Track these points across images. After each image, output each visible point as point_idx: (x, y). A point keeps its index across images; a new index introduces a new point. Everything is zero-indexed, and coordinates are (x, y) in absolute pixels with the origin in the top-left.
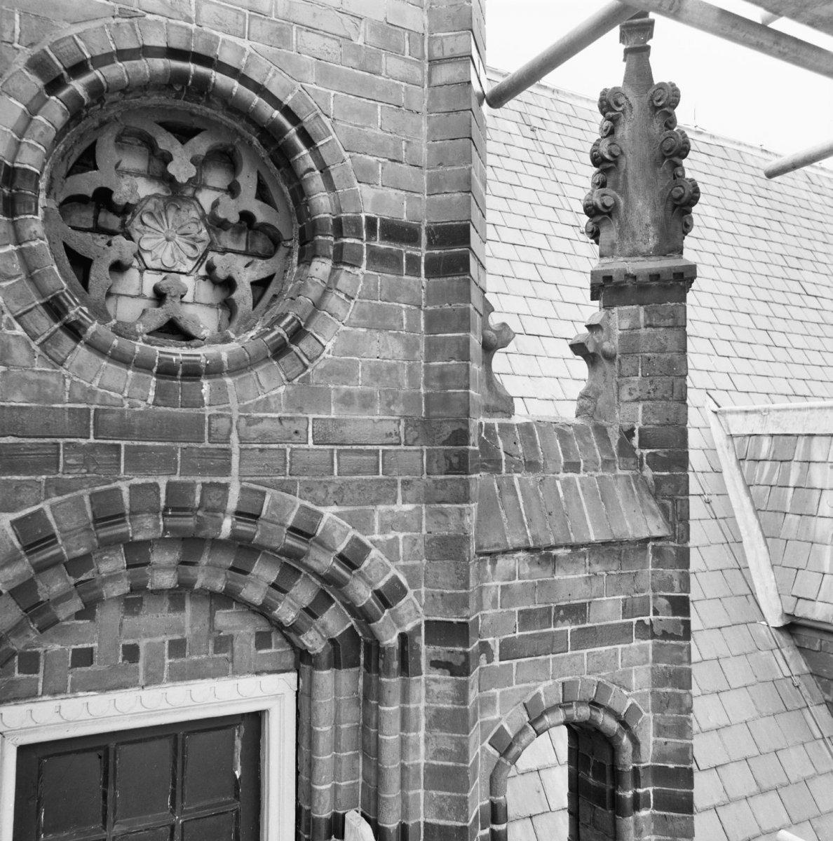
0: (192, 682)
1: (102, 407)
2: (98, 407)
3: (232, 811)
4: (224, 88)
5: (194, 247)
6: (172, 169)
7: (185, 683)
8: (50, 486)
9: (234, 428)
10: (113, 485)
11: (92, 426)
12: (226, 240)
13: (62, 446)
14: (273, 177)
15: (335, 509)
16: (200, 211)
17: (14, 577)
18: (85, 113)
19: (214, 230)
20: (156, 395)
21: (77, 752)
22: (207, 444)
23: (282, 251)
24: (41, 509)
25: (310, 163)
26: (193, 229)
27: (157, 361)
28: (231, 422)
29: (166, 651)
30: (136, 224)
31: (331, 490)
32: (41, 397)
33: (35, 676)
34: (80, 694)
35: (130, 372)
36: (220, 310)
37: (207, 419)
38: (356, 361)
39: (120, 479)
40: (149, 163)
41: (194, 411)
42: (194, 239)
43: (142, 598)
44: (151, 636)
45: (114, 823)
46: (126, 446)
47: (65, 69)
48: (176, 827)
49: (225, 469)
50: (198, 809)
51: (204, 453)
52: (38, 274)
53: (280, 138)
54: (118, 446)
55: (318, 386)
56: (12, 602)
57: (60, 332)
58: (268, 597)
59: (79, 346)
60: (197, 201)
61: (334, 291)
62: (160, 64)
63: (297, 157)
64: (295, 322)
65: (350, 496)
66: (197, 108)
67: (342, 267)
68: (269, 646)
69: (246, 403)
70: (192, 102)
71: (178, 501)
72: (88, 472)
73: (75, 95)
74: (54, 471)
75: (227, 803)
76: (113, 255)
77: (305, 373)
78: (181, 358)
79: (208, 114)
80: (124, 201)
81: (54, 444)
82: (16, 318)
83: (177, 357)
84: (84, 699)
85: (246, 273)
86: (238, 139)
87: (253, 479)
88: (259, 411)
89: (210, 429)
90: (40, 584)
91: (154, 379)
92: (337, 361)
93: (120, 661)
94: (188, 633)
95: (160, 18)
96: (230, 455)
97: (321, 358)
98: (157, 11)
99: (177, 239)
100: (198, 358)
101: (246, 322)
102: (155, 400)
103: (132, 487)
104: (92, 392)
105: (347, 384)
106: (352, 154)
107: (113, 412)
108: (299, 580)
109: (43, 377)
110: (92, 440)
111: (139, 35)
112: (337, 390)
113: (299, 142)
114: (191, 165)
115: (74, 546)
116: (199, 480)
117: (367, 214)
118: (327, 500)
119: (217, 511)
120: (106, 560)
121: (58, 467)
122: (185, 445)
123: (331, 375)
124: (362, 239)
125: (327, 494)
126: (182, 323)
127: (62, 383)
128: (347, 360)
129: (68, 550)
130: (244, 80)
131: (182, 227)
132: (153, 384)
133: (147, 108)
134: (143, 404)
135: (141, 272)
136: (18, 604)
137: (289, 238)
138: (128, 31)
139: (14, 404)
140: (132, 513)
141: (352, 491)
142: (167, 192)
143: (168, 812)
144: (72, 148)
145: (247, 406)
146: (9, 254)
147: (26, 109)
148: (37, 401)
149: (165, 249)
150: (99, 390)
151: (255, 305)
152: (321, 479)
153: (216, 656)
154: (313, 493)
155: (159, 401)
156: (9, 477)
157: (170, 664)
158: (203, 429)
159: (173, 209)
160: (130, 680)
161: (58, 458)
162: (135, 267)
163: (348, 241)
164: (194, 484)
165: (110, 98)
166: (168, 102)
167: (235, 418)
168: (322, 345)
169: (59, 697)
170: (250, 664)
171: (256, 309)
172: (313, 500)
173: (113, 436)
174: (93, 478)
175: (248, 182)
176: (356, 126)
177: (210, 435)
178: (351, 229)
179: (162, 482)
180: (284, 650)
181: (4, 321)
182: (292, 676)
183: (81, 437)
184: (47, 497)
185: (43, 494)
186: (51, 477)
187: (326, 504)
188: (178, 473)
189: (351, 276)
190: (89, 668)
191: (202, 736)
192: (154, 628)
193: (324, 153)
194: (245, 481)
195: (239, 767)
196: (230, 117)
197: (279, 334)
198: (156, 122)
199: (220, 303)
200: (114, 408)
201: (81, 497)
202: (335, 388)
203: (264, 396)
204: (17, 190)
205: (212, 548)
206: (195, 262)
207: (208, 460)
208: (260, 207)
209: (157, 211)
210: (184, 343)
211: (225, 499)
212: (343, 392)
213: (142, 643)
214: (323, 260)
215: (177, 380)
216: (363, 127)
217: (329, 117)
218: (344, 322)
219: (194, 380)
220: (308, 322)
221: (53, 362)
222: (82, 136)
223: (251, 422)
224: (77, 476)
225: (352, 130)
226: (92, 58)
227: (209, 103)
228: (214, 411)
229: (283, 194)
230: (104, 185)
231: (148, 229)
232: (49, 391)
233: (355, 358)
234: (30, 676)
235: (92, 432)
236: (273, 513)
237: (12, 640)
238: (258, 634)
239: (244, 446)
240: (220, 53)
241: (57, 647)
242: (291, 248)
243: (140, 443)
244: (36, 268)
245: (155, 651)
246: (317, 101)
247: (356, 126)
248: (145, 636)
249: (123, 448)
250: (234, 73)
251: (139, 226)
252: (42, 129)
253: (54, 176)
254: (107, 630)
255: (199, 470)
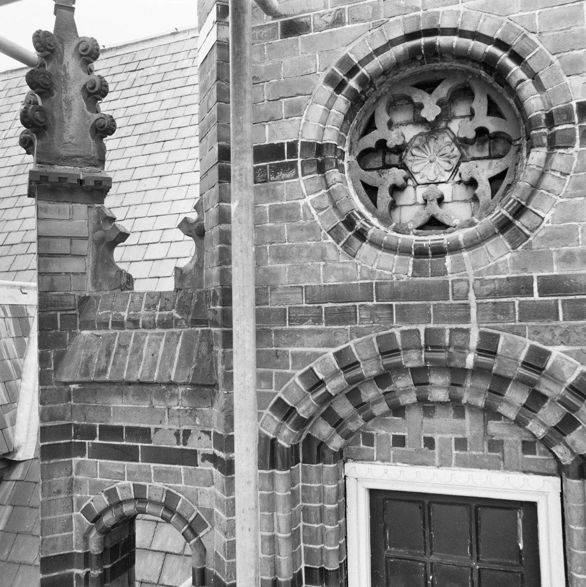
0: (473, 469)
1: (380, 281)
2: (377, 281)
3: (518, 572)
4: (446, 46)
5: (449, 162)
6: (424, 114)
7: (467, 469)
8: (353, 332)
9: (471, 288)
10: (390, 331)
11: (374, 294)
12: (473, 151)
13: (358, 307)
14: (501, 95)
15: (563, 348)
16: (452, 136)
17: (337, 386)
18: (363, 97)
19: (463, 147)
20: (413, 269)
21: (406, 501)
22: (451, 301)
23: (513, 150)
24: (349, 346)
25: (521, 75)
26: (448, 150)
27: (413, 247)
28: (469, 284)
29: (453, 445)
30: (409, 157)
31: (557, 332)
32: (347, 278)
33: (372, 448)
34: (398, 464)
35: (396, 257)
36: (473, 203)
37: (450, 283)
38: (575, 226)
39: (393, 327)
40: (414, 113)
41: (441, 278)
42: (448, 157)
43: (434, 407)
44: (442, 433)
45: (431, 553)
46: (521, 303)
47: (344, 75)
48: (474, 570)
49: (467, 318)
50: (492, 563)
51: (450, 307)
52: (338, 204)
53: (495, 65)
54: (391, 306)
55: (540, 250)
56: (347, 401)
57: (352, 237)
58: (520, 415)
59: (364, 244)
60: (449, 129)
61: (550, 172)
62: (400, 48)
63: (509, 75)
64: (516, 203)
65: (576, 337)
66: (437, 66)
67: (556, 150)
68: (535, 453)
69: (479, 269)
70: (433, 63)
71: (433, 342)
72: (374, 323)
73: (353, 90)
74: (355, 323)
75: (512, 565)
76: (390, 182)
77: (527, 241)
78: (430, 242)
79: (446, 67)
80: (394, 145)
81: (353, 306)
82: (328, 232)
83: (427, 243)
84: (401, 467)
85: (484, 171)
86: (470, 77)
87: (489, 325)
88: (490, 274)
89: (453, 290)
90: (362, 392)
91: (412, 259)
92: (556, 228)
93: (423, 447)
94: (468, 435)
95: (398, 17)
96: (469, 308)
97: (541, 227)
98: (396, 13)
99: (438, 160)
100: (441, 241)
101: (487, 208)
102: (413, 273)
103: (403, 332)
104: (372, 272)
105: (567, 245)
106: (559, 55)
107: (386, 283)
108: (546, 404)
109: (345, 266)
110: (375, 302)
111: (386, 35)
112: (558, 251)
113: (510, 63)
114: (437, 106)
115: (369, 369)
116: (447, 326)
117: (578, 101)
118: (554, 341)
119: (463, 349)
120: (400, 379)
121: (356, 320)
122: (435, 302)
123: (550, 240)
124: (574, 123)
125: (554, 336)
126: (439, 218)
127: (355, 268)
128: (566, 226)
129: (365, 372)
130: (462, 33)
131: (440, 150)
132: (411, 263)
133: (404, 79)
134: (405, 277)
135: (415, 187)
136: (351, 403)
137: (518, 137)
138: (379, 35)
139: (330, 283)
140: (404, 349)
141: (578, 334)
142: (428, 129)
143: (468, 558)
144: (361, 121)
145: (480, 271)
146: (323, 196)
147: (325, 108)
148: (342, 280)
149: (431, 166)
150: (377, 270)
151: (493, 194)
152: (547, 324)
153: (489, 454)
154: (541, 335)
155: (416, 274)
156: (331, 327)
157: (457, 454)
158: (448, 290)
159: (433, 140)
160: (430, 461)
161: (356, 314)
162: (410, 185)
163: (559, 128)
164: (444, 329)
165: (377, 82)
166: (418, 69)
167: (472, 281)
168: (541, 217)
169: (386, 463)
170: (518, 465)
171: (494, 198)
172: (541, 340)
173: (387, 299)
174: (377, 327)
175: (480, 105)
176: (562, 30)
177: (453, 294)
178: (561, 118)
179: (422, 328)
180: (547, 458)
181: (322, 235)
182: (557, 480)
183: (368, 301)
184: (352, 339)
185: (349, 336)
186: (353, 326)
187: (553, 344)
188: (432, 322)
189: (565, 156)
190: (403, 448)
191: (489, 511)
192: (444, 427)
193: (533, 64)
194: (482, 327)
195: (522, 542)
196: (461, 63)
197: (503, 214)
198: (411, 86)
199: (472, 198)
200: (387, 281)
201: (372, 338)
202: (556, 251)
203: (494, 263)
204: (324, 157)
205: (472, 375)
206: (451, 173)
207: (453, 312)
208: (491, 121)
209: (421, 144)
210: (442, 231)
211: (468, 340)
212: (563, 253)
213: (437, 437)
214: (537, 149)
215: (429, 258)
216: (570, 28)
217: (535, 33)
218: (560, 195)
219: (441, 257)
220: (528, 200)
221: (350, 256)
222: (366, 111)
223: (483, 282)
224: (367, 325)
225: (558, 35)
226: (359, 62)
227: (443, 59)
228: (455, 277)
229: (510, 105)
230: (381, 138)
231: (416, 158)
232: (348, 274)
233: (573, 223)
234: (369, 447)
235: (375, 297)
236: (507, 350)
237: (350, 423)
238: (524, 442)
239: (479, 301)
240: (441, 22)
241: (383, 432)
242: (520, 145)
243: (405, 303)
244: (337, 201)
245: (445, 443)
246: (523, 24)
247: (562, 30)
248: (438, 433)
249: (394, 307)
250: (454, 31)
251: (411, 158)
252: (334, 117)
253: (352, 141)
254: (414, 425)
255: (446, 320)
